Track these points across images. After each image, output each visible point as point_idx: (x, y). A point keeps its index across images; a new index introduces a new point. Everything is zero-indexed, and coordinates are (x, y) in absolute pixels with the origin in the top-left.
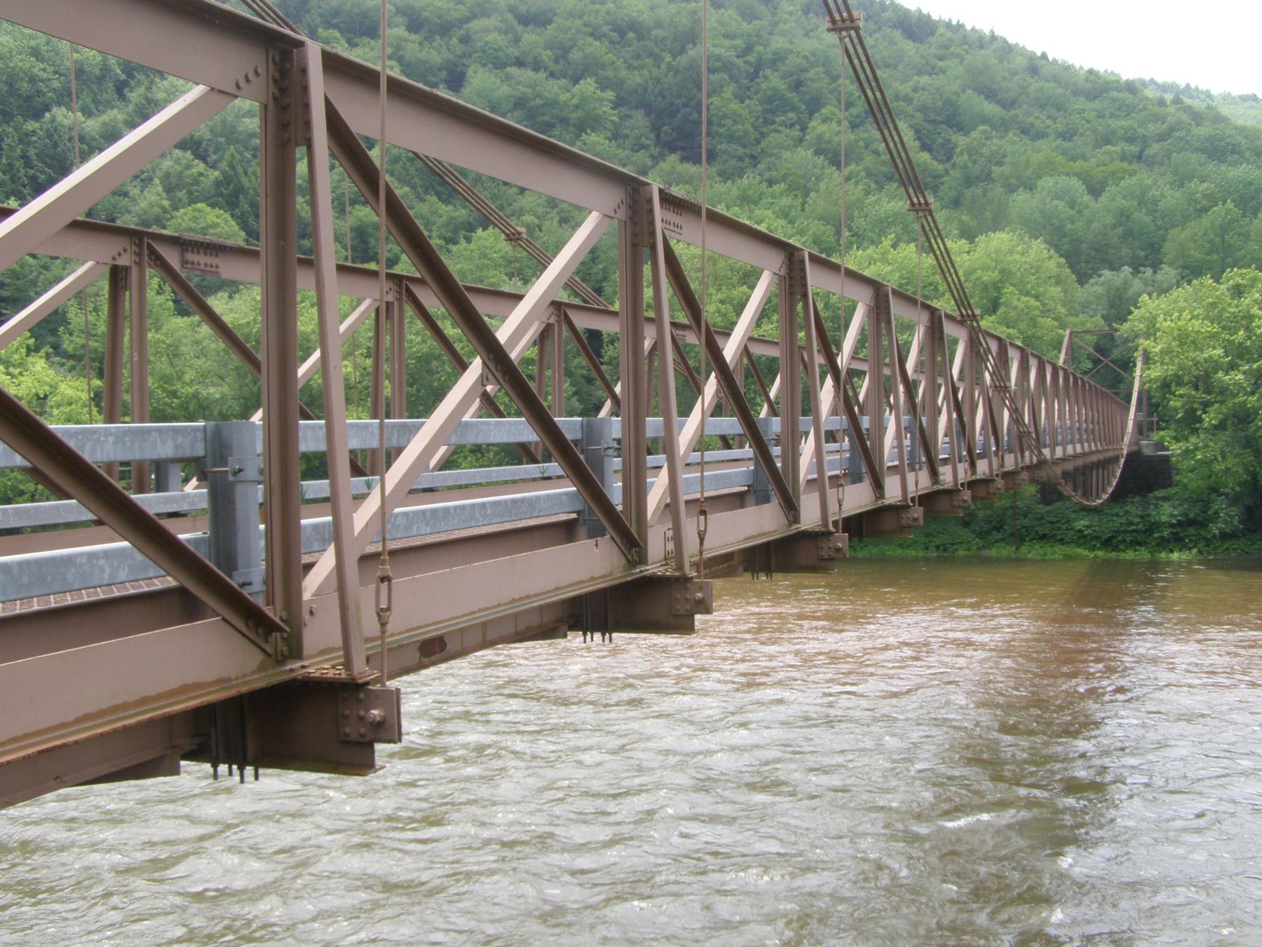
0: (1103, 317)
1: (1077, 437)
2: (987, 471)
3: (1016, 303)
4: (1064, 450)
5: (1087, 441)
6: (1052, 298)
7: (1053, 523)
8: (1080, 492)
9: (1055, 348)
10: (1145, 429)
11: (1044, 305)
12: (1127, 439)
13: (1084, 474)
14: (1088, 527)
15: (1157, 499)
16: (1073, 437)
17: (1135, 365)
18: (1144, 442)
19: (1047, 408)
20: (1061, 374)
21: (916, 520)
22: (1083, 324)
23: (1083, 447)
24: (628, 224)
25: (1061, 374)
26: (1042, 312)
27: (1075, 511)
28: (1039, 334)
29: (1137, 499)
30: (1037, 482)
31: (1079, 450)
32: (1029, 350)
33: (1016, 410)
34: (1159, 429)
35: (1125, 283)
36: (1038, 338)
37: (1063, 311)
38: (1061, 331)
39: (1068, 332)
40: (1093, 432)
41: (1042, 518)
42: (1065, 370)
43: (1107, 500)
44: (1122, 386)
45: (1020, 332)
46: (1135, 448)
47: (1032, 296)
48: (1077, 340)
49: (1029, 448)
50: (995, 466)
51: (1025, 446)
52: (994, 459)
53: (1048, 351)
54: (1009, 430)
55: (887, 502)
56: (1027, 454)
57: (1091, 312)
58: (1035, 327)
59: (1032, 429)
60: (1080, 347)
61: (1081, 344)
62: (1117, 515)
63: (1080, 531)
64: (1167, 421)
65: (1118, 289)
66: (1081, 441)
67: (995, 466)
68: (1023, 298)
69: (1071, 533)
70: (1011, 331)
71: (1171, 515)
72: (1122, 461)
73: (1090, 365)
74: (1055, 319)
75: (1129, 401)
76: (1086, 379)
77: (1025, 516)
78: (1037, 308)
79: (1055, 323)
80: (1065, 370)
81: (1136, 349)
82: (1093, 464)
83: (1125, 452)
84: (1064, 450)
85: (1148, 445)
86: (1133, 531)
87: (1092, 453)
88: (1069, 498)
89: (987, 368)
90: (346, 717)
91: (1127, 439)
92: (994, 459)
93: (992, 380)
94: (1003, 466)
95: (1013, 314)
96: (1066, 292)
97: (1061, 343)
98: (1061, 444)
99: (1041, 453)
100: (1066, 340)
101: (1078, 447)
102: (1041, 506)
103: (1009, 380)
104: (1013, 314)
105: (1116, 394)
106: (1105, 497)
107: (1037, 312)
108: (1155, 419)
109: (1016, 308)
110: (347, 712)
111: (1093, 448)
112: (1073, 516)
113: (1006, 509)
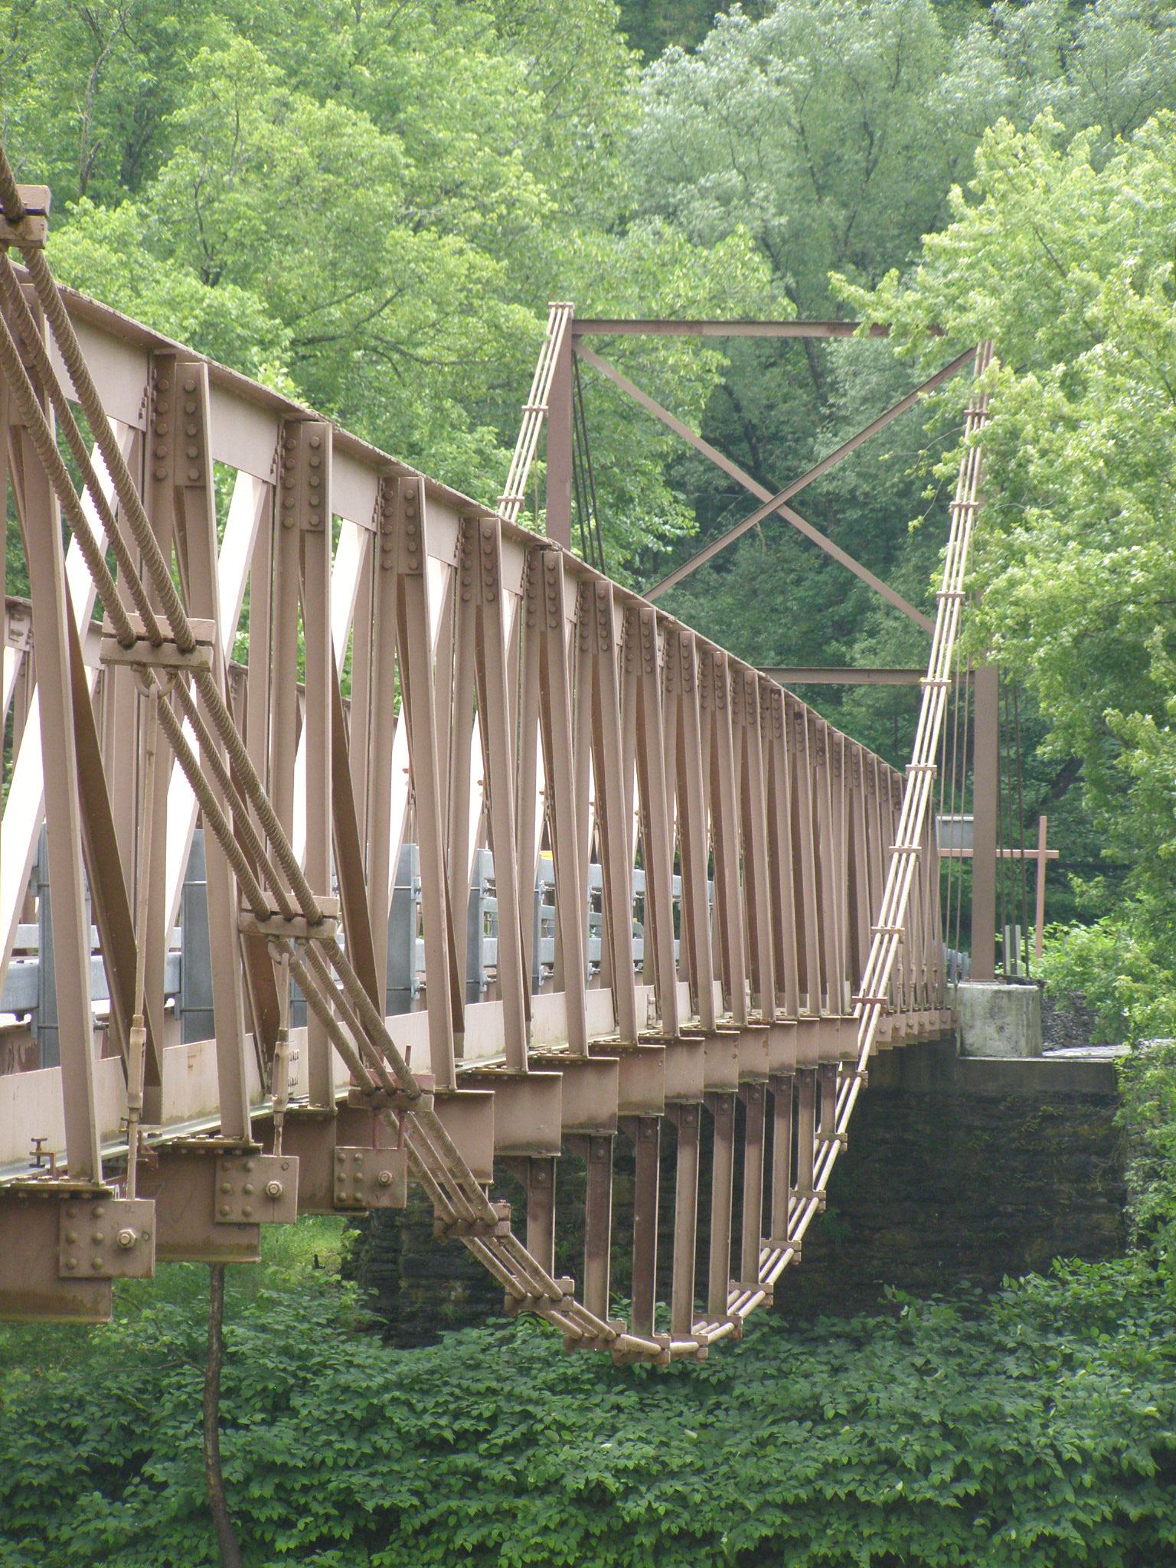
0: (764, 243)
1: (593, 946)
2: (57, 1142)
3: (260, 132)
4: (517, 1022)
5: (652, 973)
6: (476, 116)
7: (433, 1446)
8: (597, 1273)
9: (478, 412)
10: (983, 916)
11: (429, 153)
12: (876, 979)
13: (625, 1164)
14: (640, 1476)
15: (1045, 1320)
16: (567, 947)
17: (937, 531)
18: (975, 990)
19: (418, 775)
20: (511, 570)
21: (124, 1250)
22: (650, 279)
23: (622, 1011)
24: (149, 436)
25: (511, 570)
26: (413, 191)
27: (568, 1385)
28: (393, 322)
29: (939, 1315)
30: (351, 1210)
31: (599, 1026)
32: (328, 426)
33: (242, 782)
34: (1063, 913)
35: (901, 53)
36: (385, 348)
37: (535, 193)
38: (520, 315)
39: (553, 330)
40: (684, 919)
41: (375, 1419)
42: (532, 549)
43: (754, 1323)
44: (859, 653)
45: (277, 306)
46: (921, 1022)
47: (360, 100)
48: (606, 370)
49: (311, 1004)
50: (106, 1111)
51: (286, 993)
52: (102, 1071)
53: (440, 423)
54: (190, 895)
55: (168, 1135)
56: (297, 1042)
57: (706, 211)
58: (371, 281)
59: (330, 901)
60: (629, 415)
61: (633, 395)
62: (811, 1413)
63: (596, 1499)
64: (1115, 871)
65: (857, 84)
66: (610, 974)
67: (106, 1111)
68: (307, 109)
69: (543, 1510)
70: (226, 296)
71: (1124, 1420)
72: (850, 1092)
73: (682, 522)
74: (485, 240)
75: (898, 750)
76: (723, 653)
77: (278, 1406)
78: (389, 172)
79: (489, 266)
80: (532, 549)
81: (951, 434)
82: (676, 1106)
83: (865, 1043)
84: (517, 1022)
85: (995, 1008)
86: (899, 1506)
87: (676, 1042)
88: (534, 1307)
89: (75, 523)
90: (225, 1192)
91: (876, 979)
92: (102, 1071)
93: (105, 601)
94: (151, 1113)
95: (244, 197)
96: (555, 86)
97: (516, 382)
98: (495, 991)
99: (375, 1037)
100: (546, 367)
101: (597, 1006)
102: (368, 1351)
103: (209, 609)
104: (244, 197)
105: (833, 696)
106: (744, 1303)
107: (385, 196)
108: (1044, 853)
109: (261, 163)
110: (227, 1186)
111: (685, 1019)
112: (557, 1409)
113: (165, 1360)
